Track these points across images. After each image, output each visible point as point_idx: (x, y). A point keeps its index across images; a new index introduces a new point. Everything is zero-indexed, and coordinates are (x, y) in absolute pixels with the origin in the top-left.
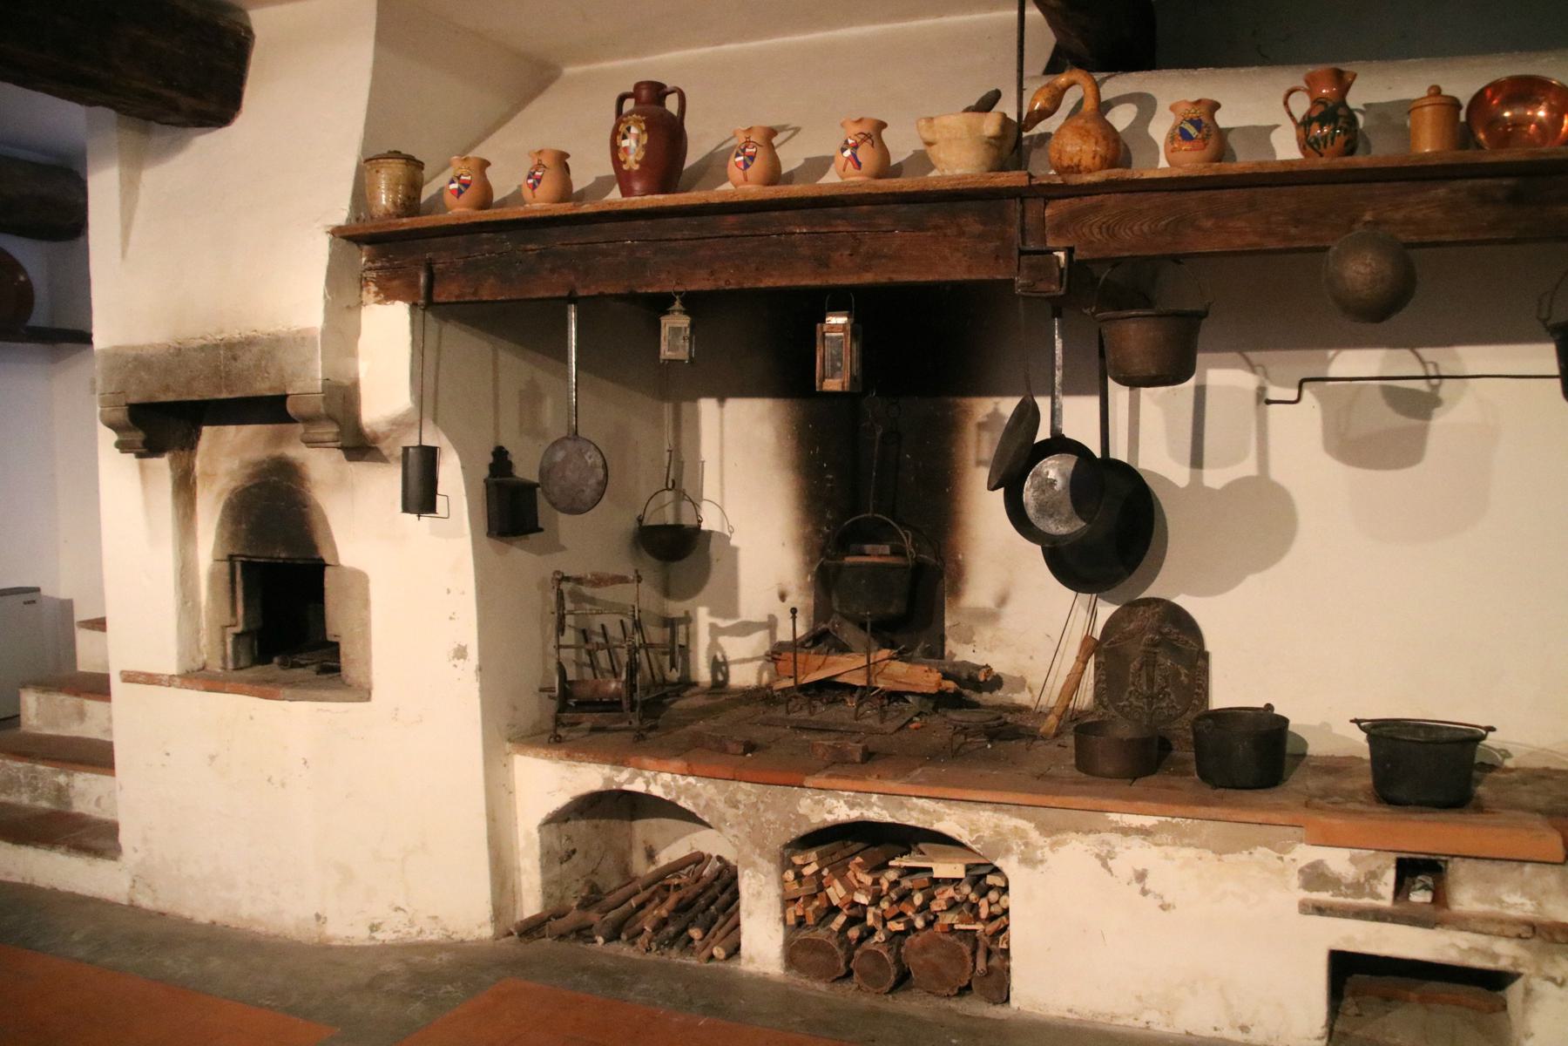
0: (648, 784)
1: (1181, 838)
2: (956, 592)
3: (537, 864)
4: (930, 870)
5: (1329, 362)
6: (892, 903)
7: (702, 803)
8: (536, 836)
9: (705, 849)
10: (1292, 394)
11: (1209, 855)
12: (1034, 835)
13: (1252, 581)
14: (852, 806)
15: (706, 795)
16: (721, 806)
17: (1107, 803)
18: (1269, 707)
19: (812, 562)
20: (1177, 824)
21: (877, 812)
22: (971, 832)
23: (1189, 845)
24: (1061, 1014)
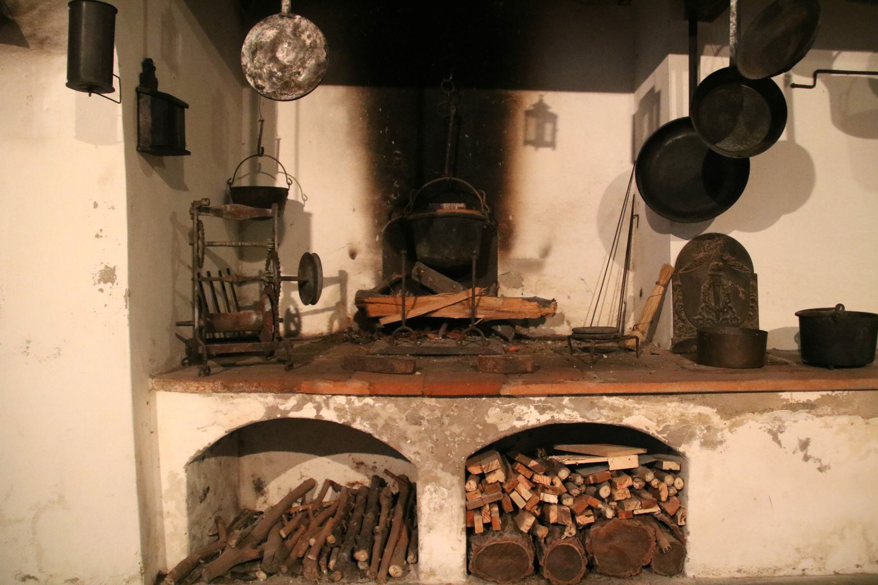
0: (318, 408)
1: (838, 408)
2: (507, 246)
3: (184, 506)
4: (606, 464)
5: (833, 59)
6: (576, 498)
7: (380, 422)
8: (183, 476)
9: (309, 475)
10: (809, 81)
11: (859, 420)
12: (716, 419)
13: (785, 219)
14: (542, 410)
15: (384, 415)
16: (402, 424)
17: (784, 383)
18: (839, 305)
19: (380, 225)
20: (836, 397)
21: (568, 413)
22: (659, 422)
23: (845, 413)
24: (731, 575)
